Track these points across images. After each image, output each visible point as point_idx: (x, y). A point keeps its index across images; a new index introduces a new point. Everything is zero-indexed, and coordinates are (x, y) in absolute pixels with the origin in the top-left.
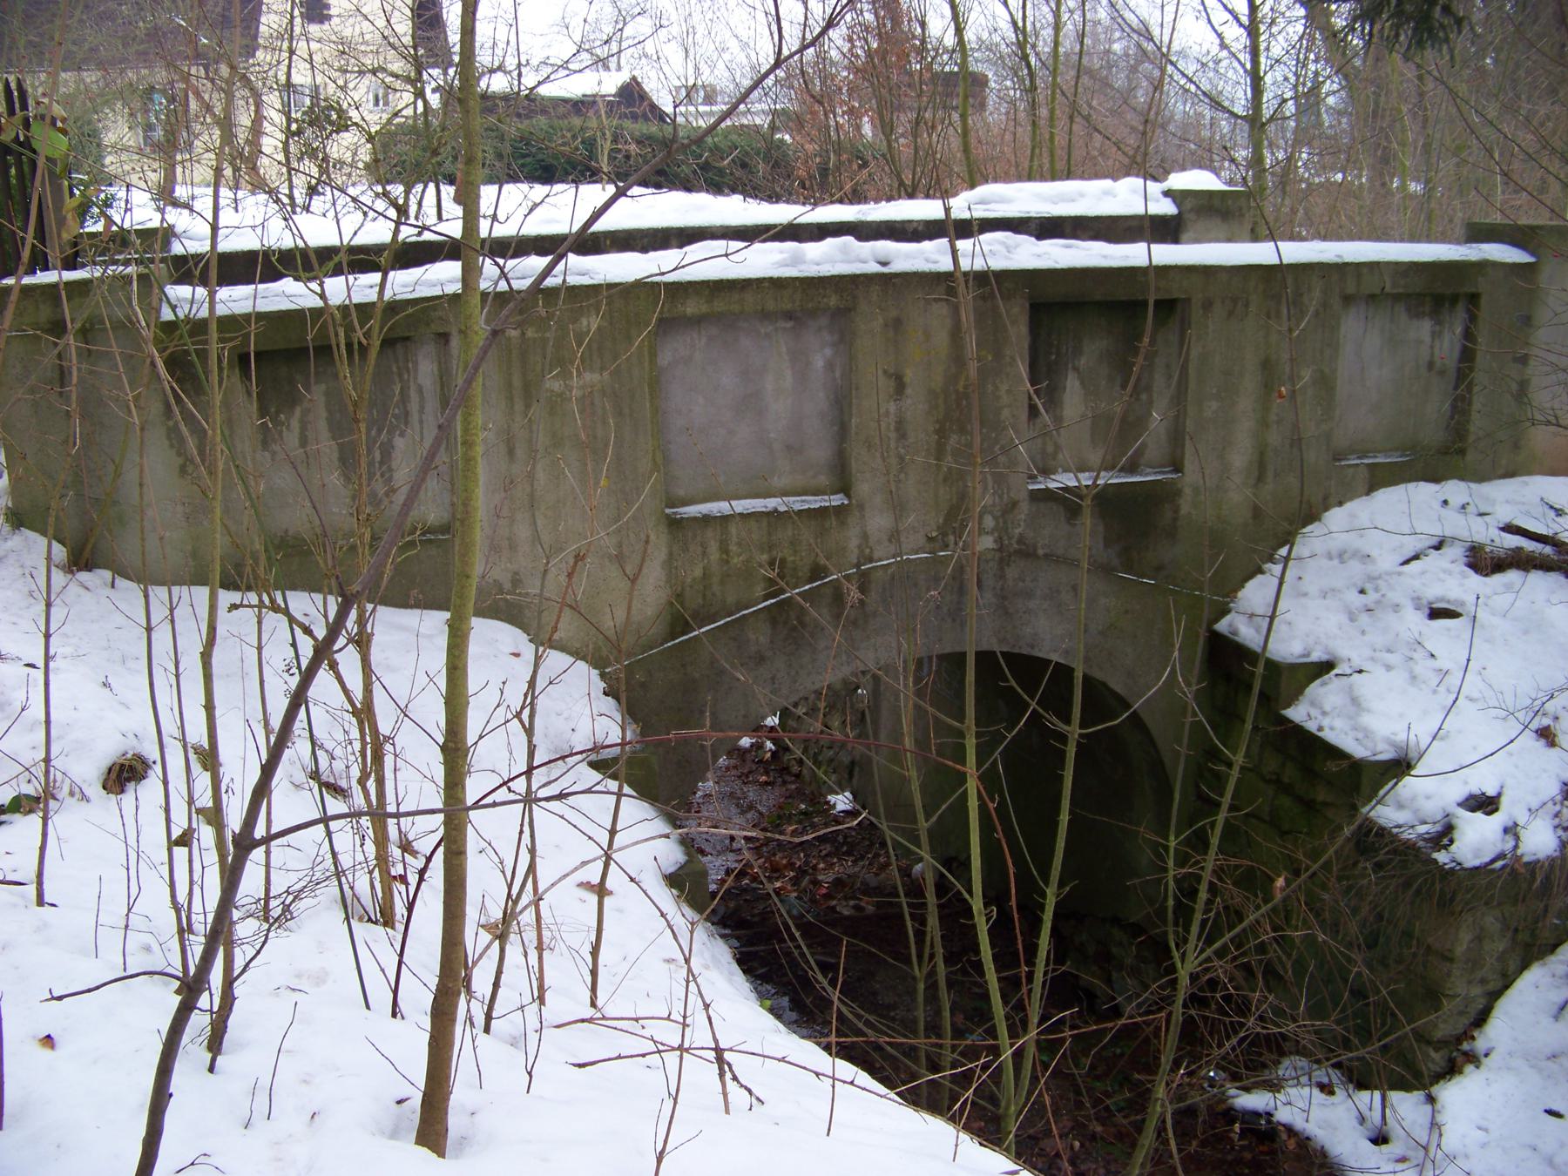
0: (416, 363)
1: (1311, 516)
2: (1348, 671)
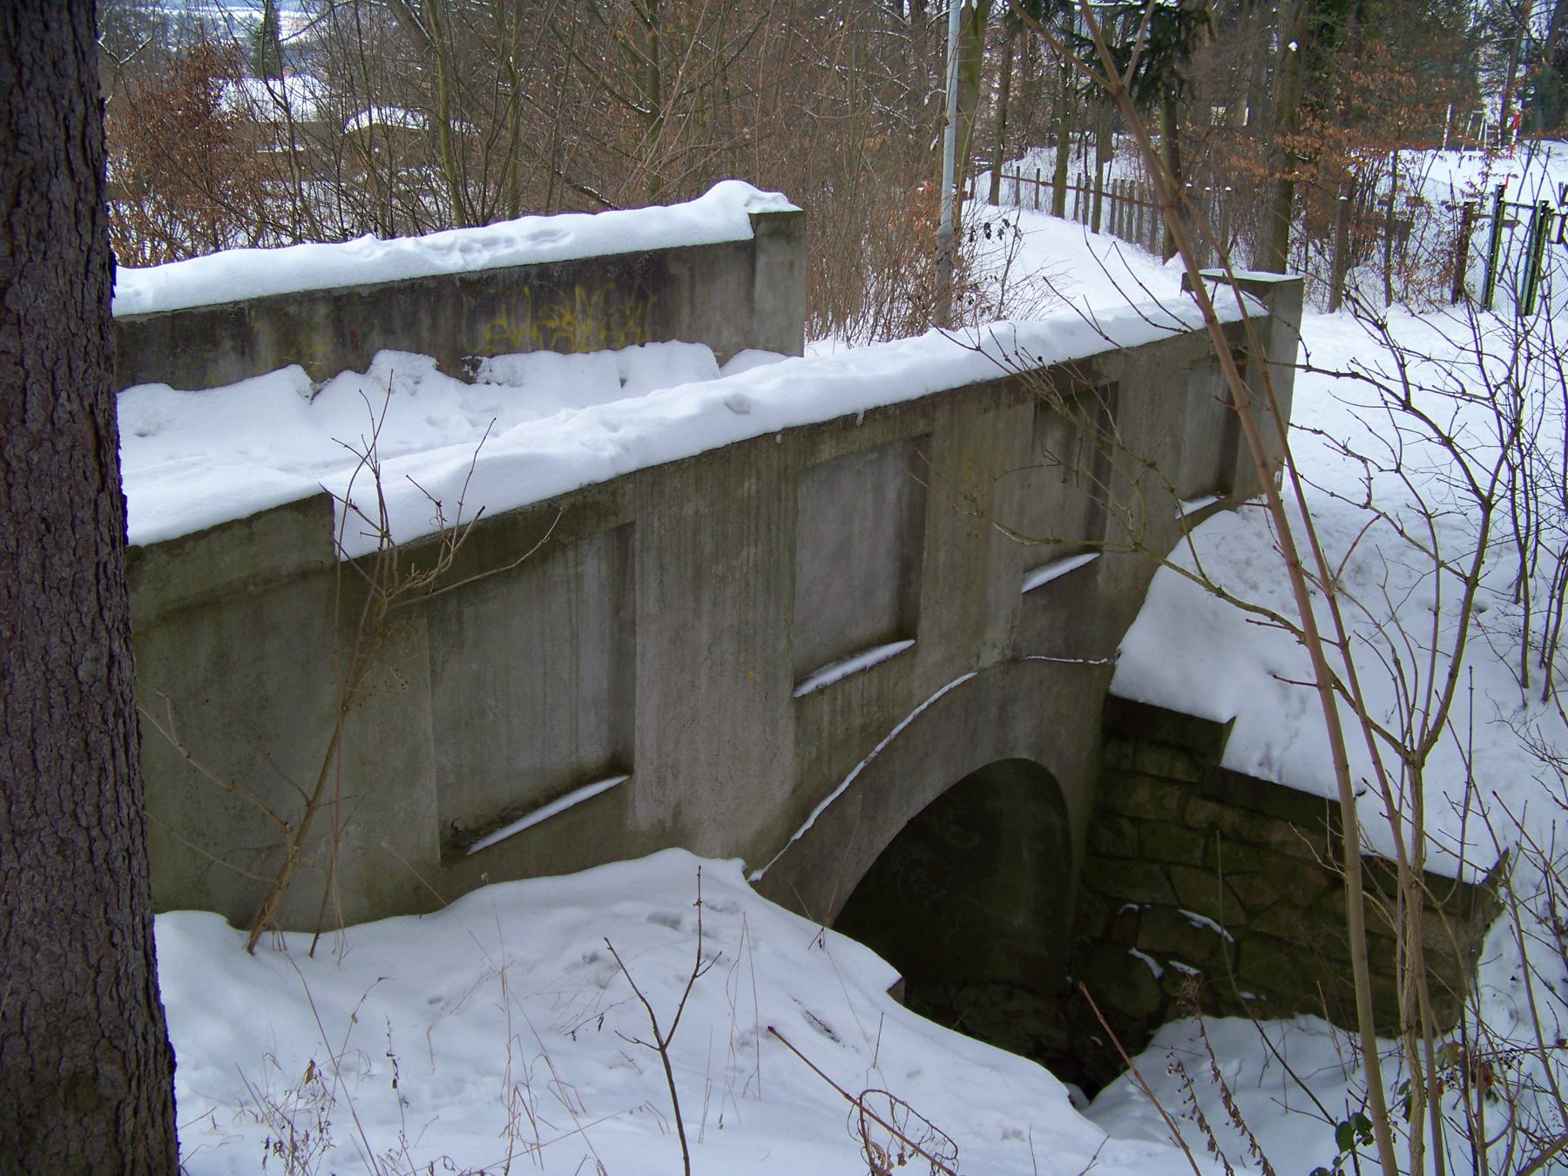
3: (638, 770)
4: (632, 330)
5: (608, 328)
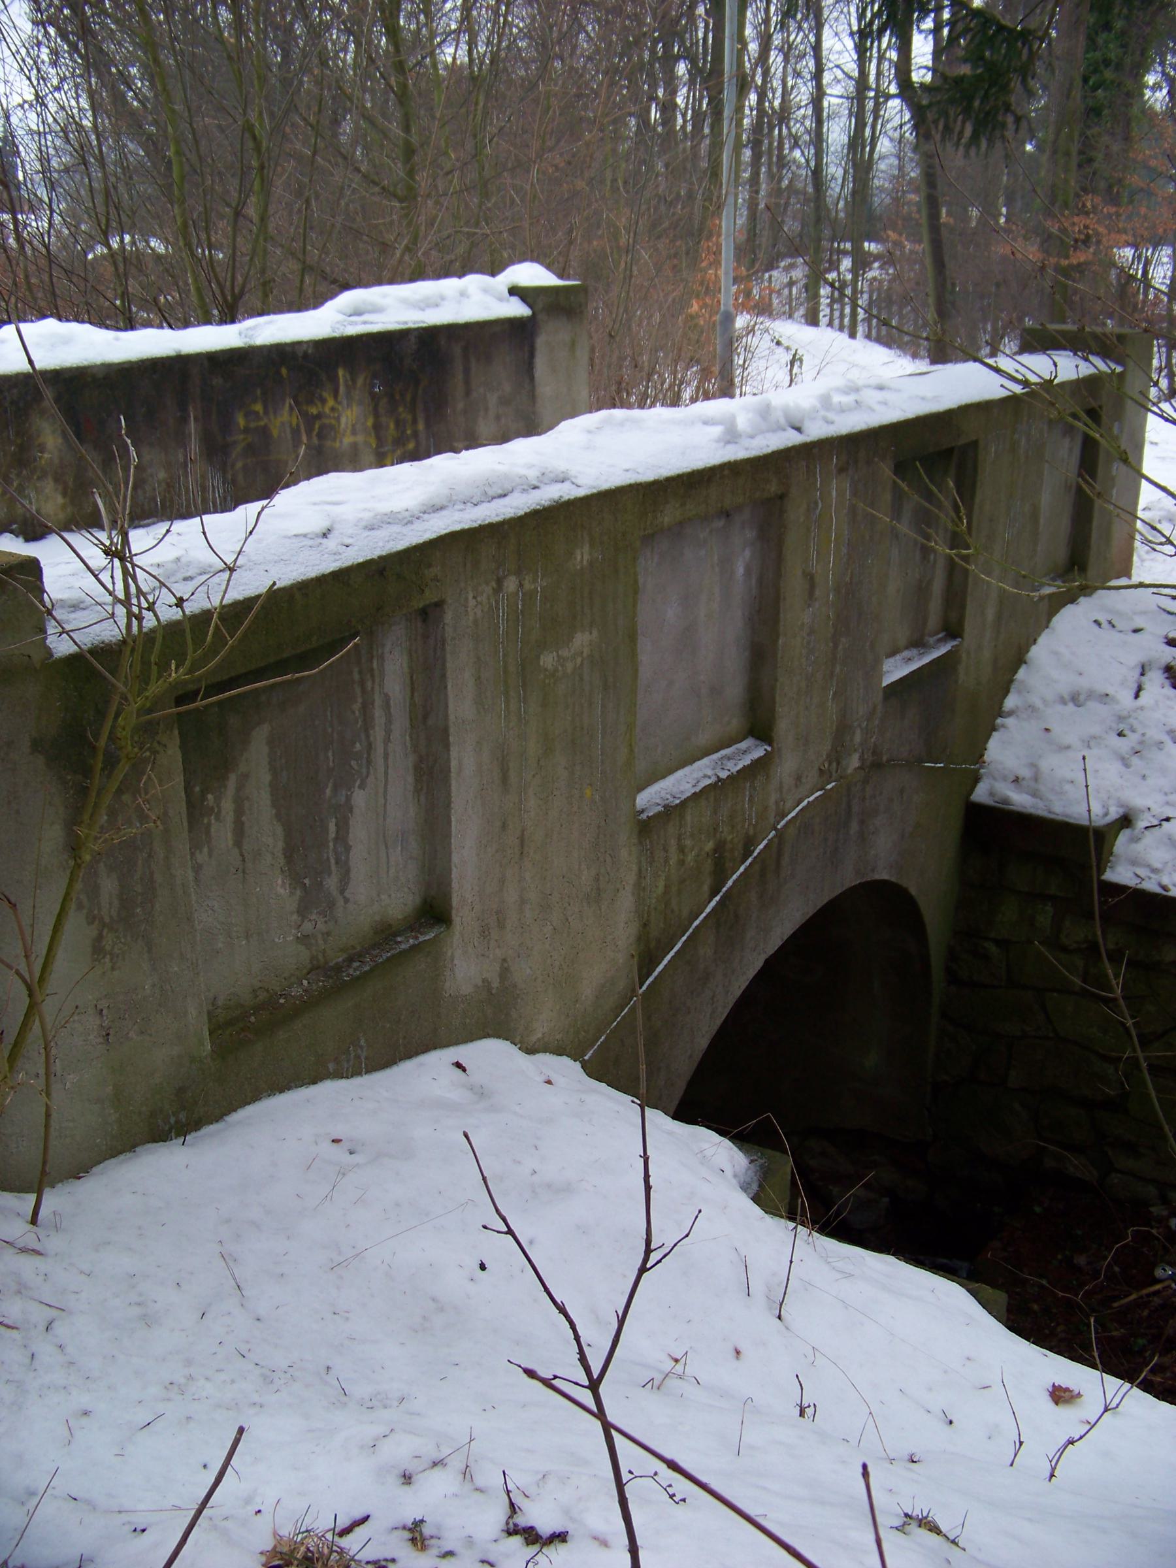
0: (382, 658)
1: (1019, 659)
2: (1156, 822)
3: (456, 919)
4: (403, 416)
5: (377, 415)
